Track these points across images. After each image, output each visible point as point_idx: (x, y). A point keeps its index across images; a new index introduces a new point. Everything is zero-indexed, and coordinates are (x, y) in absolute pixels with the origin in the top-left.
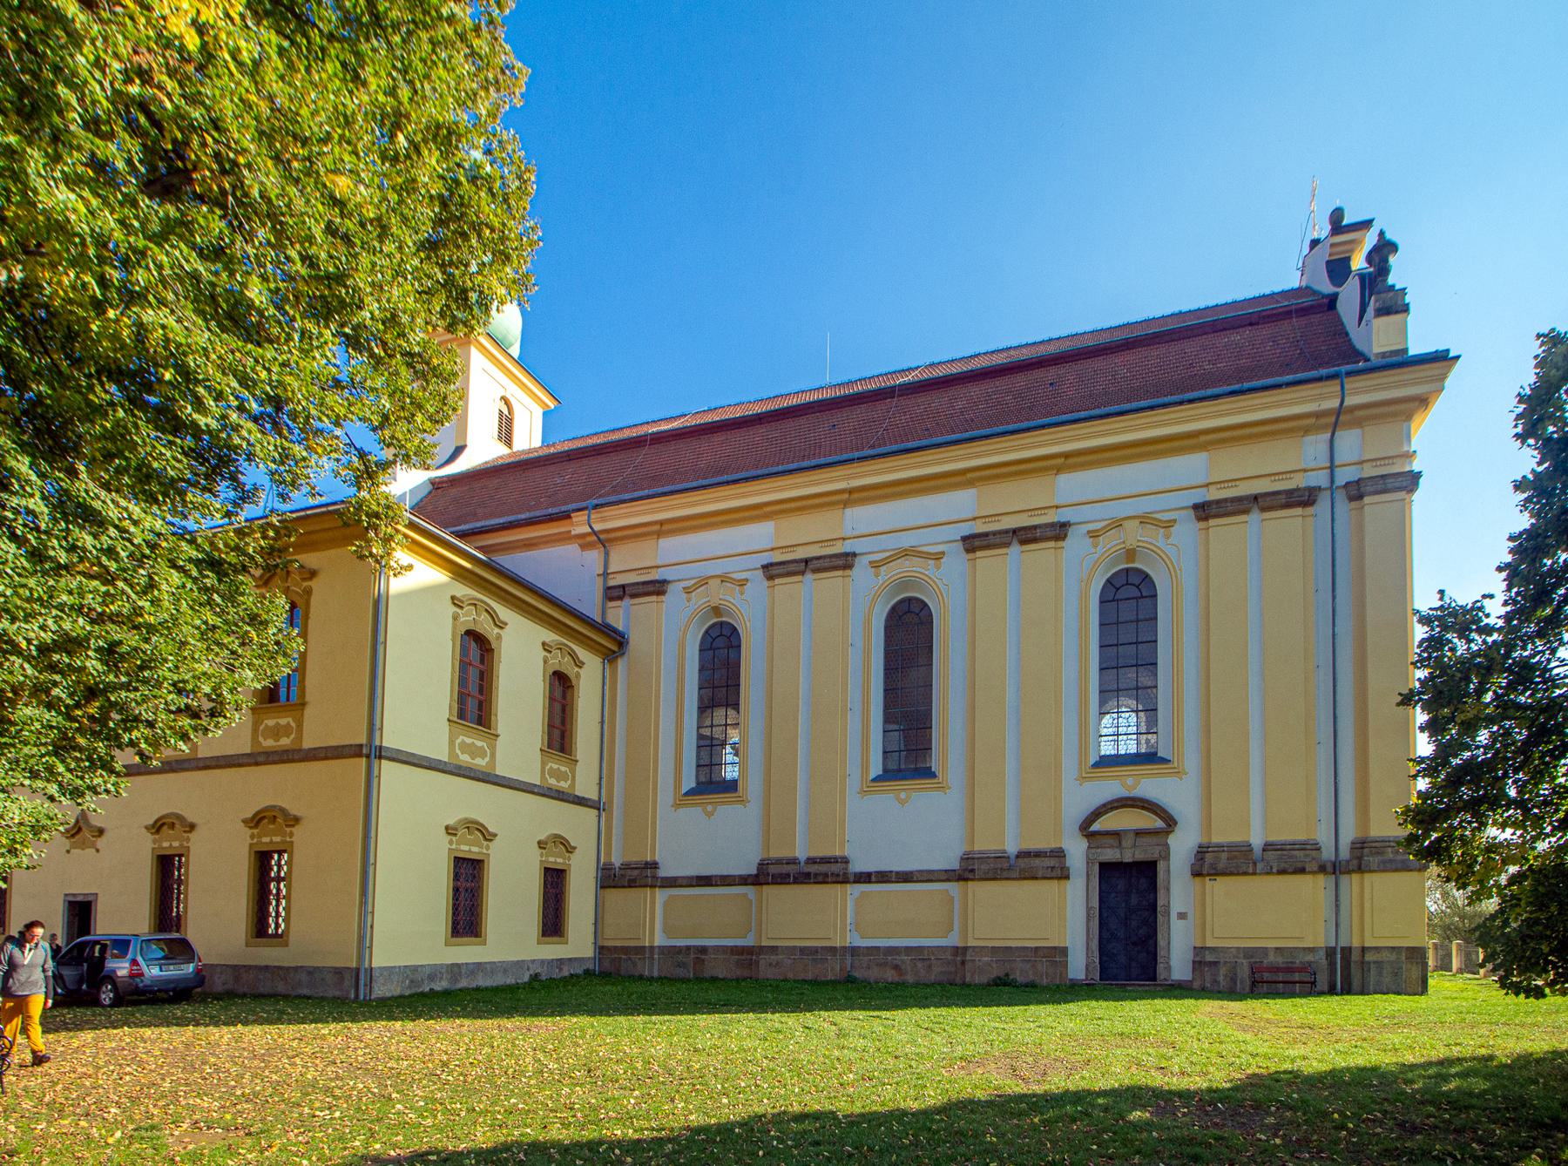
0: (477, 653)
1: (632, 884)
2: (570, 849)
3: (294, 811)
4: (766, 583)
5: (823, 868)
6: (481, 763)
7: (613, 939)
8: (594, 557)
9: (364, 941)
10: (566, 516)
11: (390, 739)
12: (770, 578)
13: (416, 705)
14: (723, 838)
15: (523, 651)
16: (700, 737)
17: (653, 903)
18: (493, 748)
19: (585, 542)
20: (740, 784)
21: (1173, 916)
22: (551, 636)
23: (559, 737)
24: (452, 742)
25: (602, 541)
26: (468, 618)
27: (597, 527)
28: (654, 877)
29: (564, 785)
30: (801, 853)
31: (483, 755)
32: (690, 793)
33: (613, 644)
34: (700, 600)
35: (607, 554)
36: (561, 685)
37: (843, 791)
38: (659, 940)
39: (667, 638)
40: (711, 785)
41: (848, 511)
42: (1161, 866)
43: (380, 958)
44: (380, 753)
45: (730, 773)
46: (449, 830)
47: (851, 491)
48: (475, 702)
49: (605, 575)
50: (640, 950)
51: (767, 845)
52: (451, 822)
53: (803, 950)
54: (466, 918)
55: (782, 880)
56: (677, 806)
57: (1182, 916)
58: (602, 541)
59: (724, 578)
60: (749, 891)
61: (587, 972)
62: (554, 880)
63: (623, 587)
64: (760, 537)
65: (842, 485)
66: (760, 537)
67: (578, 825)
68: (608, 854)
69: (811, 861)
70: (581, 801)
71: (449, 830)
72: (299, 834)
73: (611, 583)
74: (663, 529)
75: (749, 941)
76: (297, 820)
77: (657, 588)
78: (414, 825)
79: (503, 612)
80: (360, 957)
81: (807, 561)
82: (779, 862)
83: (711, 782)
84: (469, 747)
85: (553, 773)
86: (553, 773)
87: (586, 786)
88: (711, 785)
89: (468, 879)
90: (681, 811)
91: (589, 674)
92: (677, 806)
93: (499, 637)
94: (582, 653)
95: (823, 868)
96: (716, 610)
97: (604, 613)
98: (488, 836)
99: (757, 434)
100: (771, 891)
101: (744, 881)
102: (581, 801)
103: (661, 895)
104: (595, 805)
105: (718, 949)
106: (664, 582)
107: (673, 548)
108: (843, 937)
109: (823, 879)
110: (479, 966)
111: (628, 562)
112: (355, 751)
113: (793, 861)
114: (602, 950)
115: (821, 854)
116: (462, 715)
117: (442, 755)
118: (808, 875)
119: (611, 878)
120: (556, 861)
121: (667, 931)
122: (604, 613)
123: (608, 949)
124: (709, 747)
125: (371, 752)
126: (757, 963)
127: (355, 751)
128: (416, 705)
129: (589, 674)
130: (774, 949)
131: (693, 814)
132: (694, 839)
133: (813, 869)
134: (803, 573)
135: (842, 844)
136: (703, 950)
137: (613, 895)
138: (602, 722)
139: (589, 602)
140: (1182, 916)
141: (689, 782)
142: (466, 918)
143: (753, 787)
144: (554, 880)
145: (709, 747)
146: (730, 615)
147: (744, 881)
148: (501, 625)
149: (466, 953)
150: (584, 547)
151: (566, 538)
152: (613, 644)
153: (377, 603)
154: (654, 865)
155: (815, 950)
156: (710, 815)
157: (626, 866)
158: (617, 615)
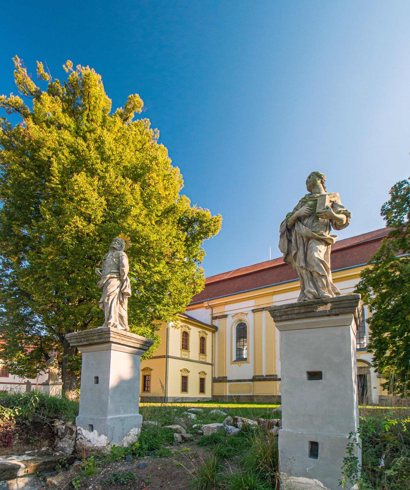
0: (185, 335)
1: (220, 381)
2: (205, 374)
3: (151, 368)
4: (253, 314)
5: (270, 377)
6: (187, 357)
7: (216, 394)
8: (209, 311)
9: (166, 392)
10: (203, 302)
11: (170, 354)
12: (254, 312)
13: (175, 346)
14: (246, 371)
15: (195, 334)
16: (237, 348)
17: (226, 386)
18: (189, 354)
19: (207, 308)
20: (248, 359)
21: (372, 388)
22: (200, 330)
23: (203, 351)
24: (181, 354)
25: (211, 307)
26: (184, 329)
27: (210, 304)
28: (226, 380)
29: (204, 360)
30: (264, 374)
31: (187, 355)
32: (235, 361)
33: (214, 329)
34: (236, 318)
35: (212, 309)
36: (203, 340)
37: (275, 360)
38: (228, 394)
39: (229, 327)
40: (240, 359)
41: (274, 296)
42: (368, 375)
43: (169, 395)
44: (168, 357)
45: (245, 357)
46: (181, 371)
47: (274, 292)
48: (185, 346)
49: (212, 314)
50: (223, 396)
51: (255, 372)
52: (181, 369)
53: (265, 396)
54: (184, 388)
55: (260, 380)
56: (231, 364)
57: (375, 388)
58: (211, 307)
59: (242, 313)
60: (251, 383)
61: (210, 401)
62: (202, 381)
63: (217, 317)
64: (252, 304)
65: (272, 291)
66: (252, 304)
67: (208, 369)
68: (215, 375)
69: (267, 376)
70: (208, 364)
71: (181, 371)
72: (152, 373)
73: (213, 316)
74: (226, 303)
75: (251, 394)
76: (152, 369)
77: (225, 316)
78: (175, 369)
79: (190, 327)
80: (165, 395)
81: (263, 308)
82: (258, 376)
83: (240, 358)
84: (184, 354)
85: (202, 358)
86: (202, 358)
87: (209, 360)
88: (240, 359)
89: (185, 379)
90: (232, 365)
91: (209, 336)
92: (231, 364)
93: (190, 332)
94: (207, 332)
95: (270, 377)
96: (240, 320)
97: (212, 322)
98: (188, 372)
99: (249, 278)
100: (256, 383)
101: (249, 380)
102: (208, 364)
103: (228, 384)
104: (212, 365)
105: (243, 396)
106: (227, 315)
107: (227, 308)
108: (276, 393)
109: (270, 380)
110: (187, 398)
111: (217, 311)
112: (164, 357)
113: (262, 376)
114: (213, 396)
115: (270, 374)
116: (183, 348)
117: (179, 356)
118: (266, 379)
119: (215, 380)
120: (202, 377)
121: (230, 392)
122: (212, 322)
123: (215, 396)
124: (239, 351)
125: (167, 357)
126: (253, 399)
127: (164, 357)
128: (175, 346)
129: (209, 336)
130: (257, 396)
131: (236, 366)
132: (234, 371)
133: (268, 377)
134: (262, 311)
135: (275, 372)
136: (239, 396)
137: (216, 384)
138: (212, 346)
139: (209, 322)
140: (375, 388)
141: (234, 358)
142: (184, 388)
143: (251, 359)
144: (202, 381)
145: (239, 351)
146: (243, 321)
147: (249, 380)
148: (190, 329)
149: (185, 395)
150: (206, 309)
151: (202, 307)
152: (214, 329)
153: (167, 329)
154: (226, 377)
155: (269, 396)
156: (240, 366)
157: (219, 378)
158: (216, 323)
